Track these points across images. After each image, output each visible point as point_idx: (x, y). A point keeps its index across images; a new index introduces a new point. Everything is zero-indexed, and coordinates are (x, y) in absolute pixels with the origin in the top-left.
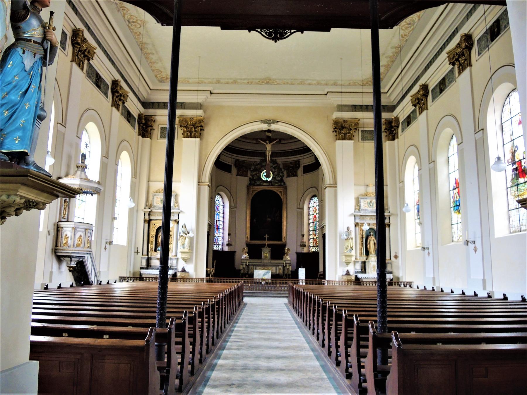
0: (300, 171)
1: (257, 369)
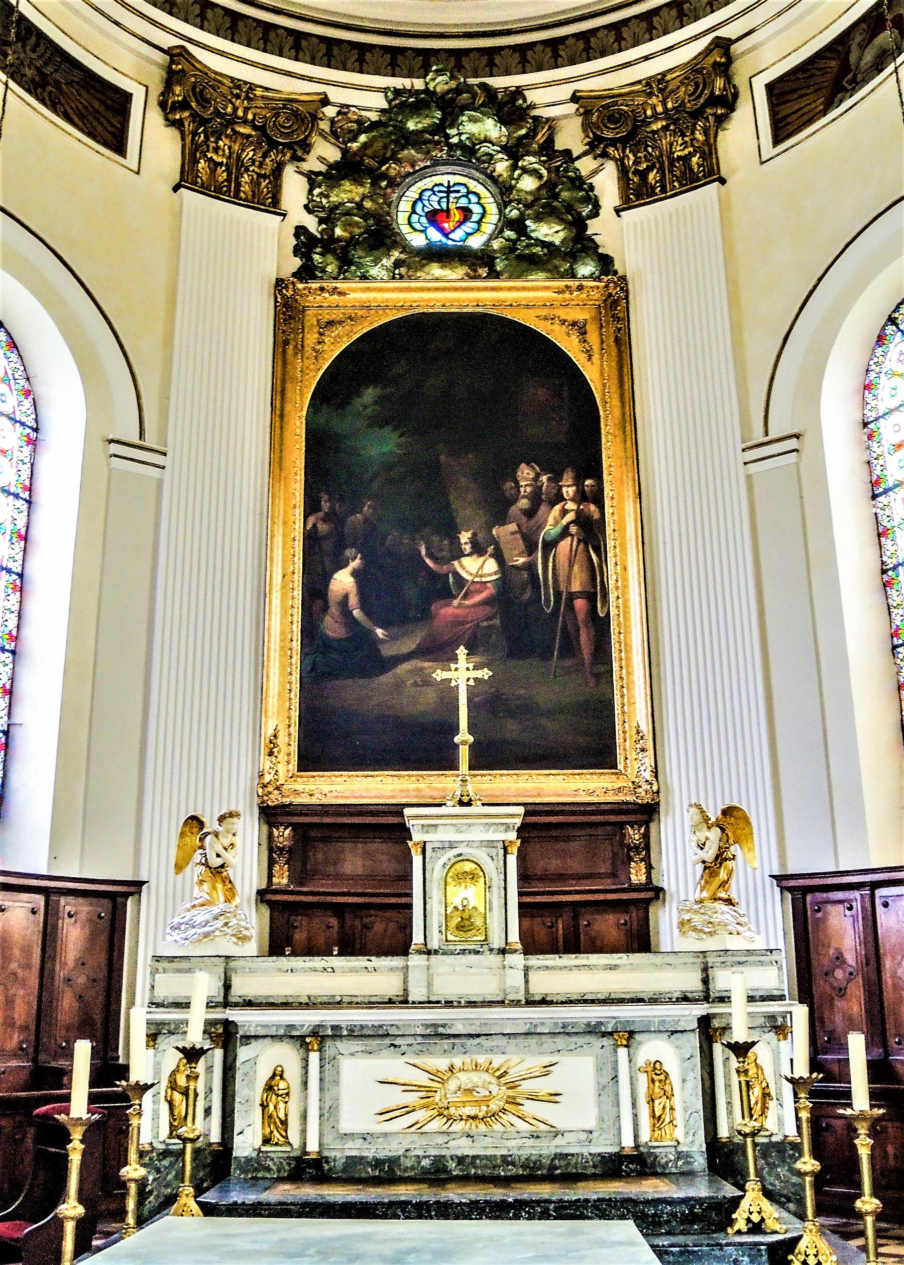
0: (743, 135)
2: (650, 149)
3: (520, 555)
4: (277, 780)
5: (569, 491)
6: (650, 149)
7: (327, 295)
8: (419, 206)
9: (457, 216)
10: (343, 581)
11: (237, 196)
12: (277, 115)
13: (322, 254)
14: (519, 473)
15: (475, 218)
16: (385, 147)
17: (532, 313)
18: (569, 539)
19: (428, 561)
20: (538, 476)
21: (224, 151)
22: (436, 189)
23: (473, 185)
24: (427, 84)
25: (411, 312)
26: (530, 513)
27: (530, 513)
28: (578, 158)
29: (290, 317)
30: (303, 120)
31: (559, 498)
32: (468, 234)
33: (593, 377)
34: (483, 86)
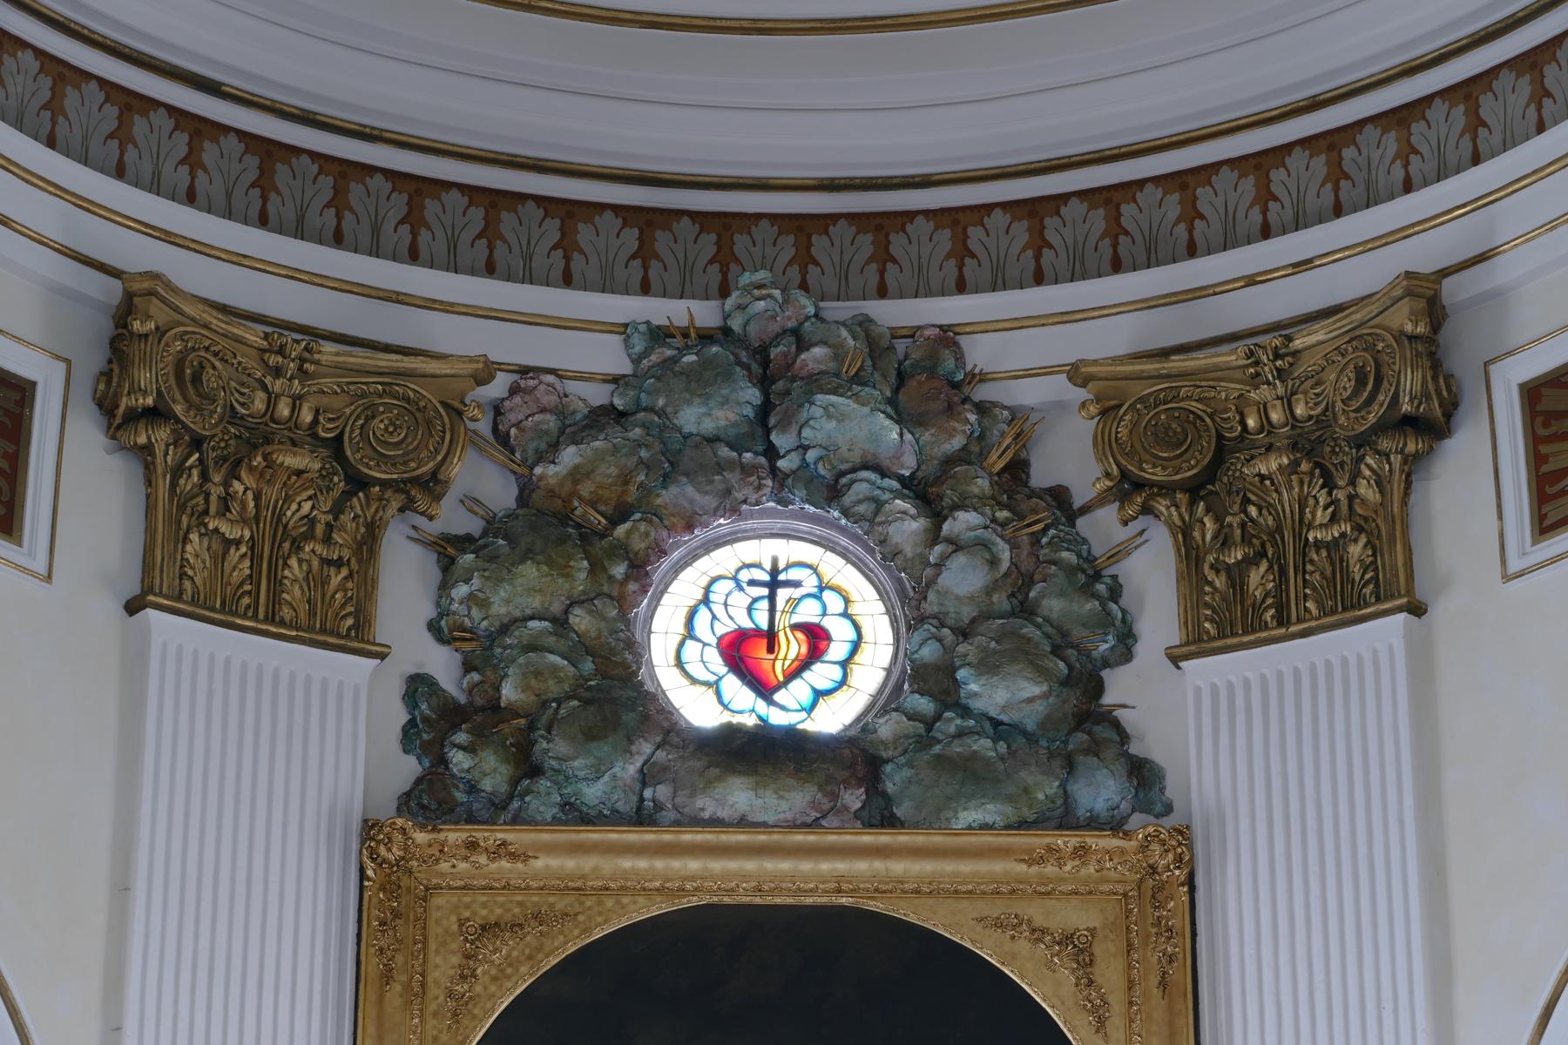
2: (1253, 511)
6: (1253, 511)
7: (483, 859)
8: (703, 616)
9: (792, 647)
11: (271, 618)
12: (370, 413)
13: (469, 749)
15: (837, 651)
16: (625, 478)
21: (243, 504)
22: (745, 576)
24: (726, 317)
28: (1085, 510)
29: (396, 914)
30: (429, 424)
32: (819, 694)
34: (864, 324)
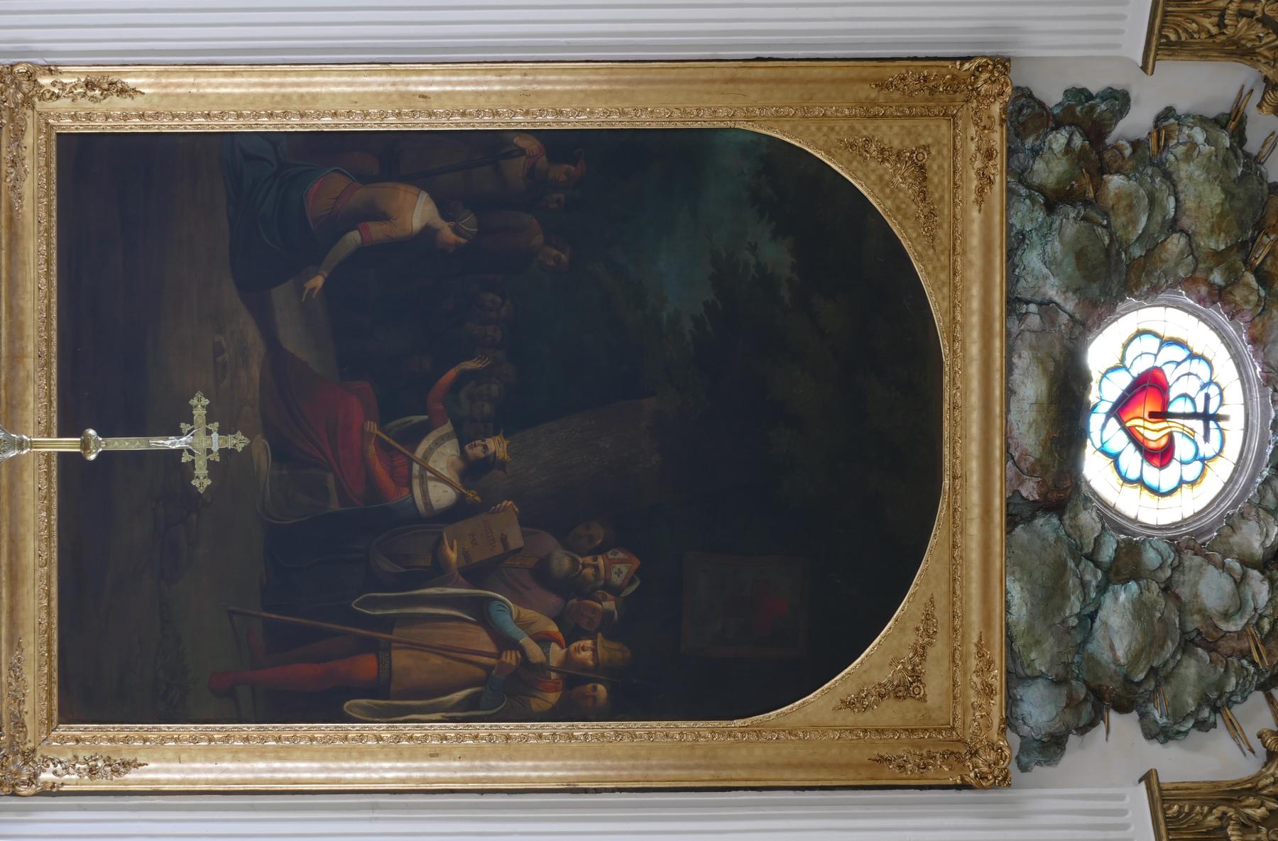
1: (629, 82)
3: (464, 554)
4: (41, 98)
5: (585, 651)
7: (978, 164)
9: (1154, 434)
10: (419, 212)
14: (621, 555)
15: (1152, 475)
17: (940, 592)
18: (491, 648)
19: (452, 373)
20: (615, 591)
23: (1221, 472)
25: (943, 343)
26: (542, 574)
27: (542, 574)
29: (933, 90)
31: (572, 634)
32: (1115, 458)
33: (809, 709)
